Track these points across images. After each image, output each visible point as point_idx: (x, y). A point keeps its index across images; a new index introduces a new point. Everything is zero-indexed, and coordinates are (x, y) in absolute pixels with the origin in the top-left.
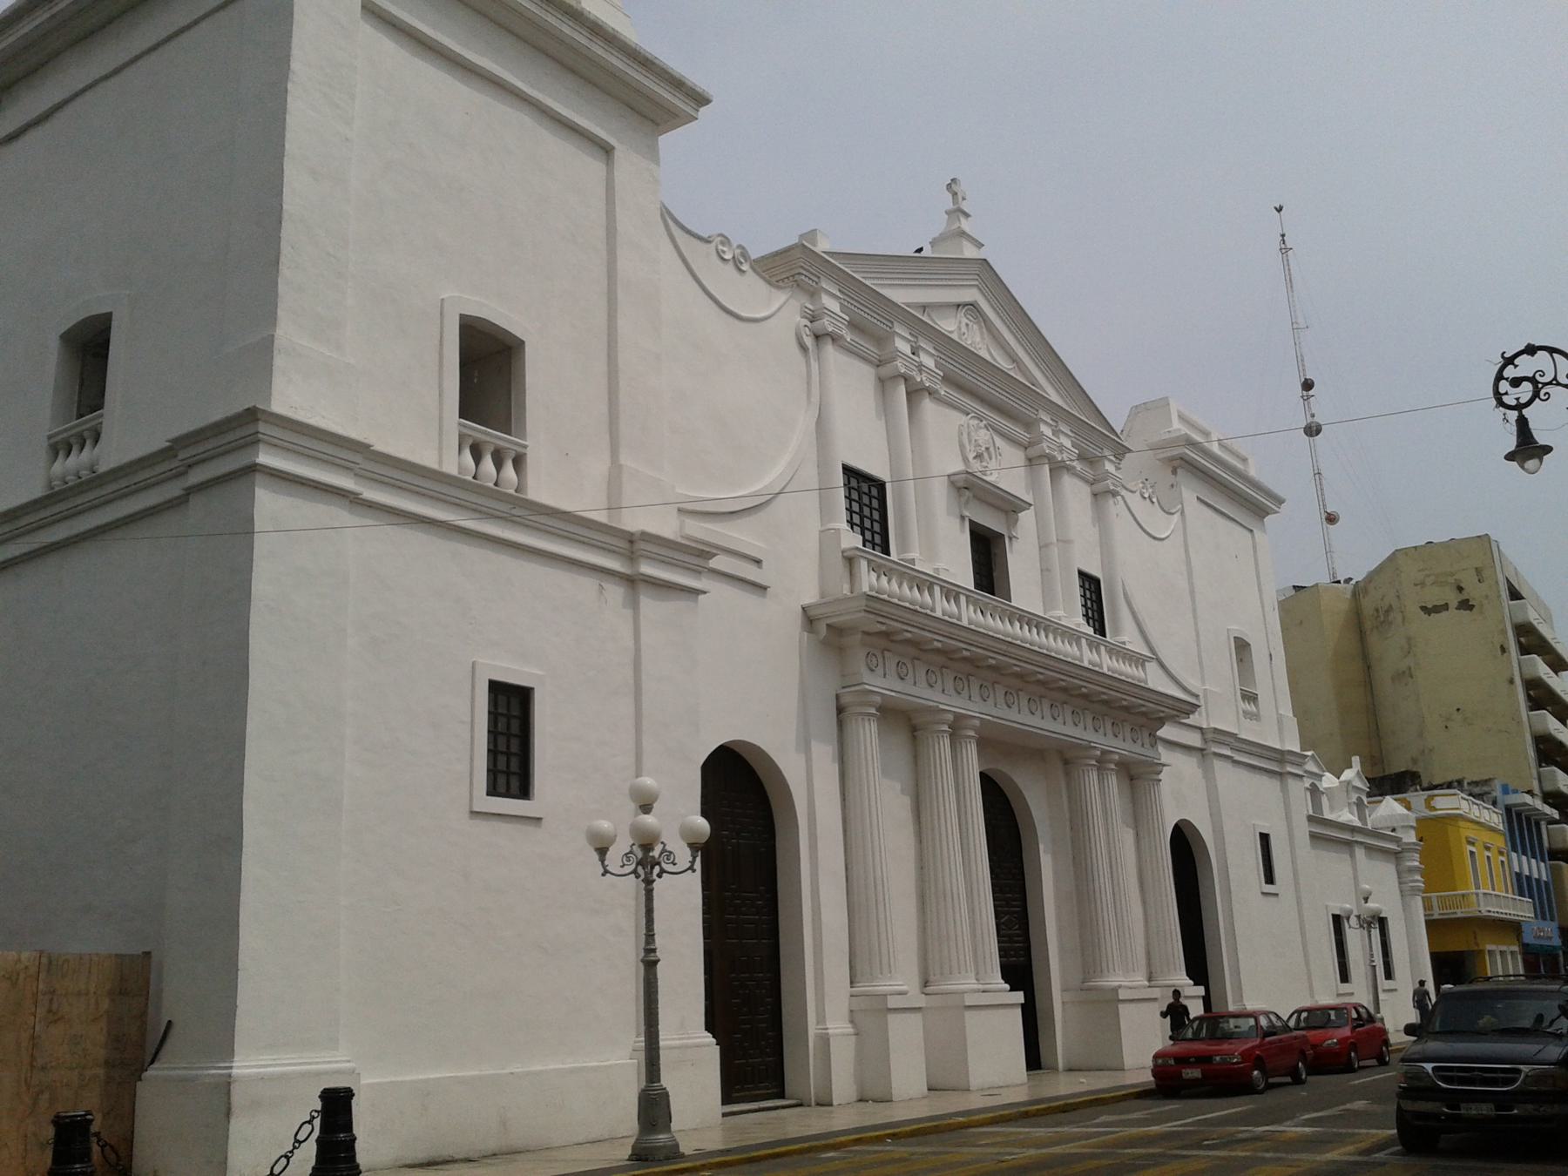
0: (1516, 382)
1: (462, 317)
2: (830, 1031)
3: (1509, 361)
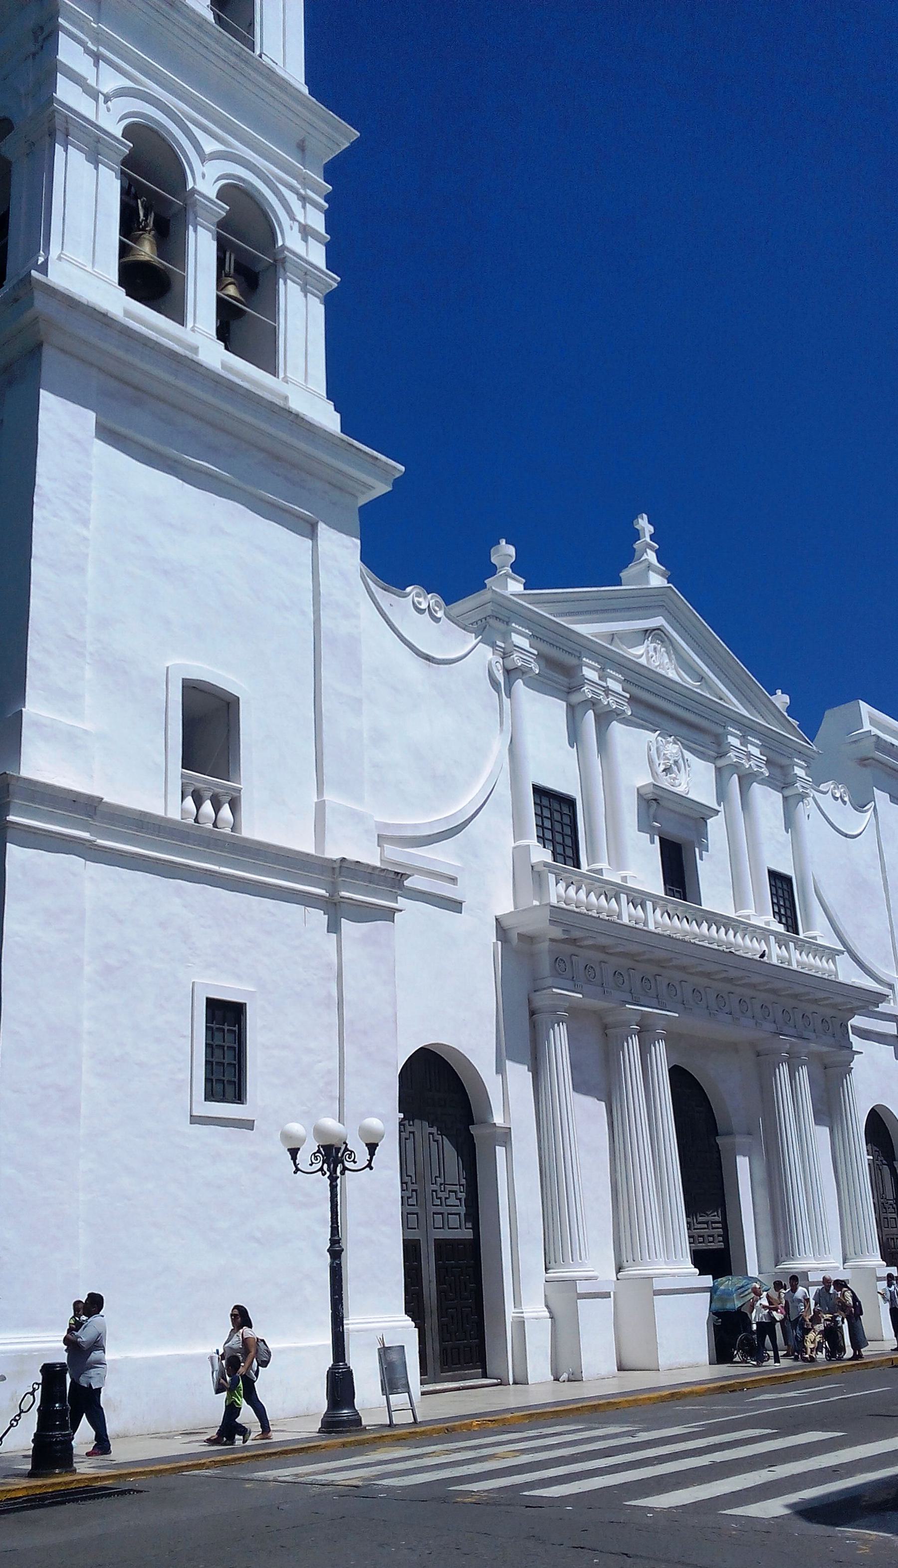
2: (525, 1315)
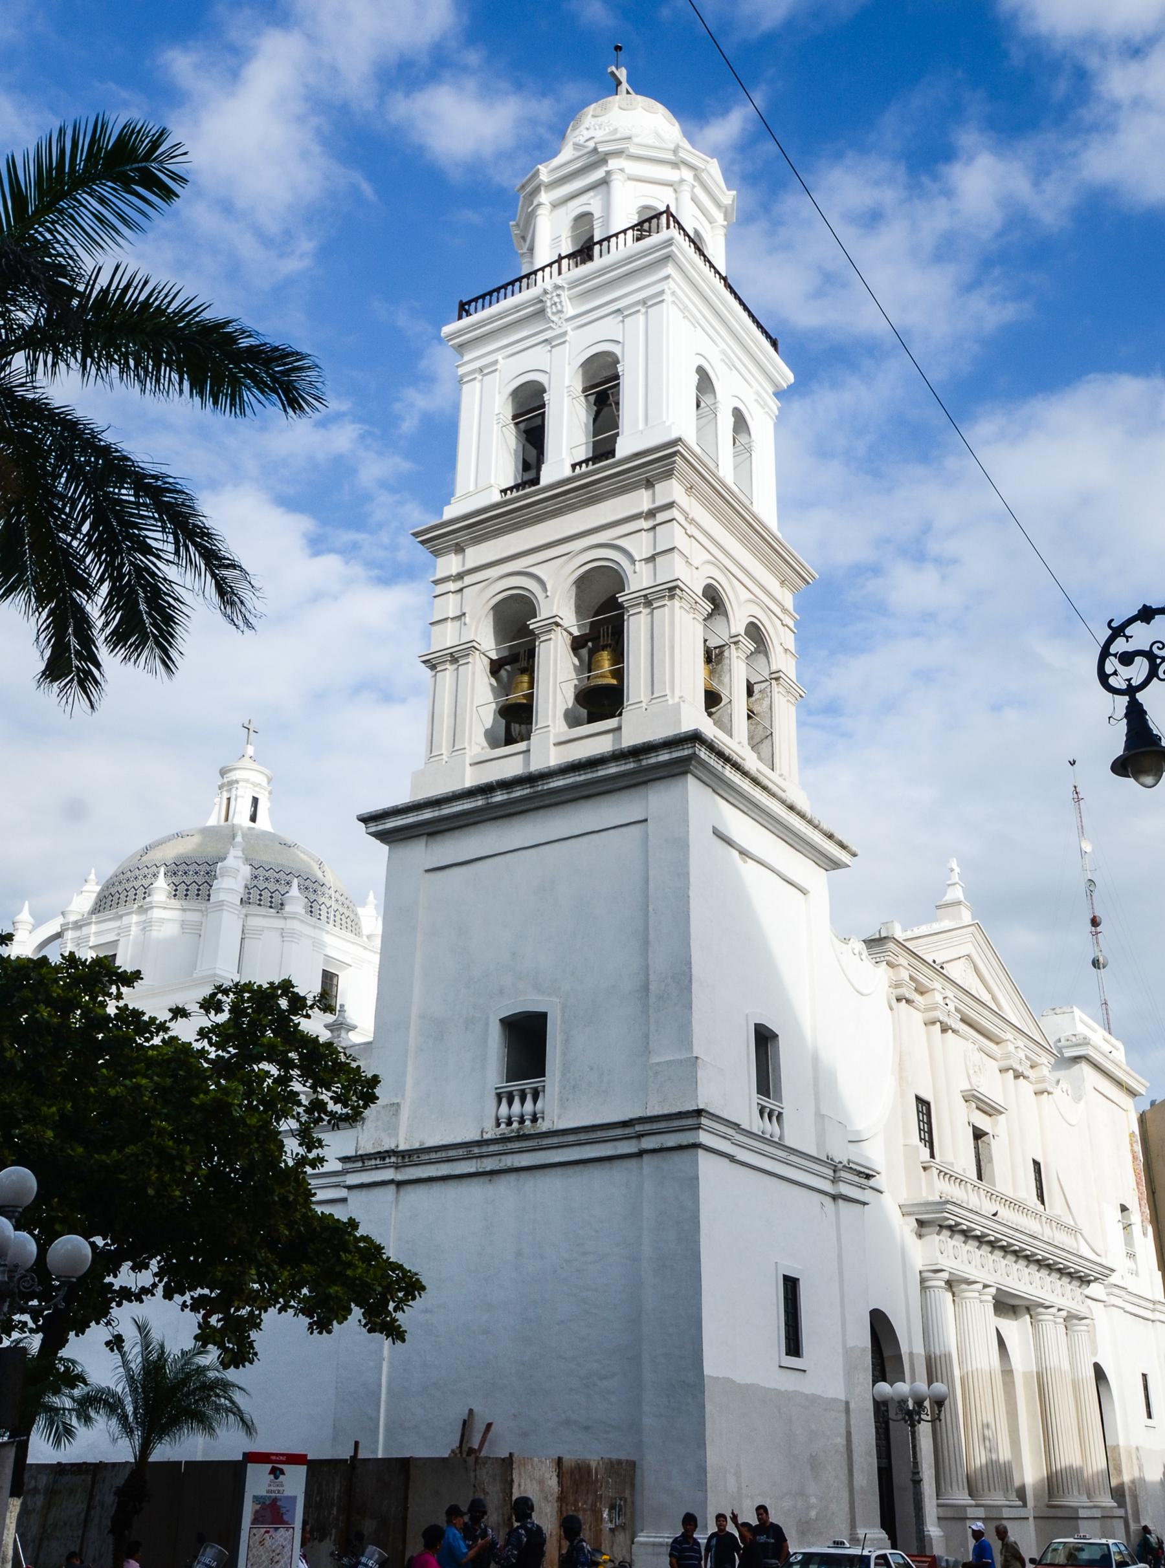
0: (1127, 659)
1: (755, 1024)
3: (1118, 631)
